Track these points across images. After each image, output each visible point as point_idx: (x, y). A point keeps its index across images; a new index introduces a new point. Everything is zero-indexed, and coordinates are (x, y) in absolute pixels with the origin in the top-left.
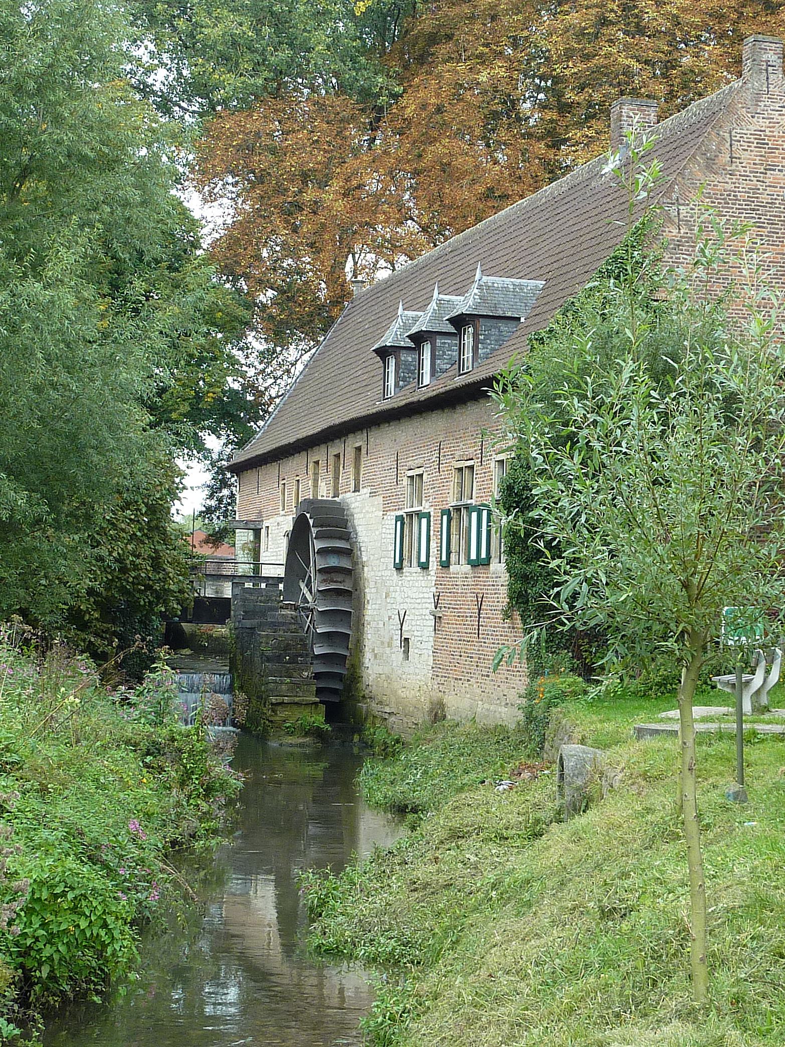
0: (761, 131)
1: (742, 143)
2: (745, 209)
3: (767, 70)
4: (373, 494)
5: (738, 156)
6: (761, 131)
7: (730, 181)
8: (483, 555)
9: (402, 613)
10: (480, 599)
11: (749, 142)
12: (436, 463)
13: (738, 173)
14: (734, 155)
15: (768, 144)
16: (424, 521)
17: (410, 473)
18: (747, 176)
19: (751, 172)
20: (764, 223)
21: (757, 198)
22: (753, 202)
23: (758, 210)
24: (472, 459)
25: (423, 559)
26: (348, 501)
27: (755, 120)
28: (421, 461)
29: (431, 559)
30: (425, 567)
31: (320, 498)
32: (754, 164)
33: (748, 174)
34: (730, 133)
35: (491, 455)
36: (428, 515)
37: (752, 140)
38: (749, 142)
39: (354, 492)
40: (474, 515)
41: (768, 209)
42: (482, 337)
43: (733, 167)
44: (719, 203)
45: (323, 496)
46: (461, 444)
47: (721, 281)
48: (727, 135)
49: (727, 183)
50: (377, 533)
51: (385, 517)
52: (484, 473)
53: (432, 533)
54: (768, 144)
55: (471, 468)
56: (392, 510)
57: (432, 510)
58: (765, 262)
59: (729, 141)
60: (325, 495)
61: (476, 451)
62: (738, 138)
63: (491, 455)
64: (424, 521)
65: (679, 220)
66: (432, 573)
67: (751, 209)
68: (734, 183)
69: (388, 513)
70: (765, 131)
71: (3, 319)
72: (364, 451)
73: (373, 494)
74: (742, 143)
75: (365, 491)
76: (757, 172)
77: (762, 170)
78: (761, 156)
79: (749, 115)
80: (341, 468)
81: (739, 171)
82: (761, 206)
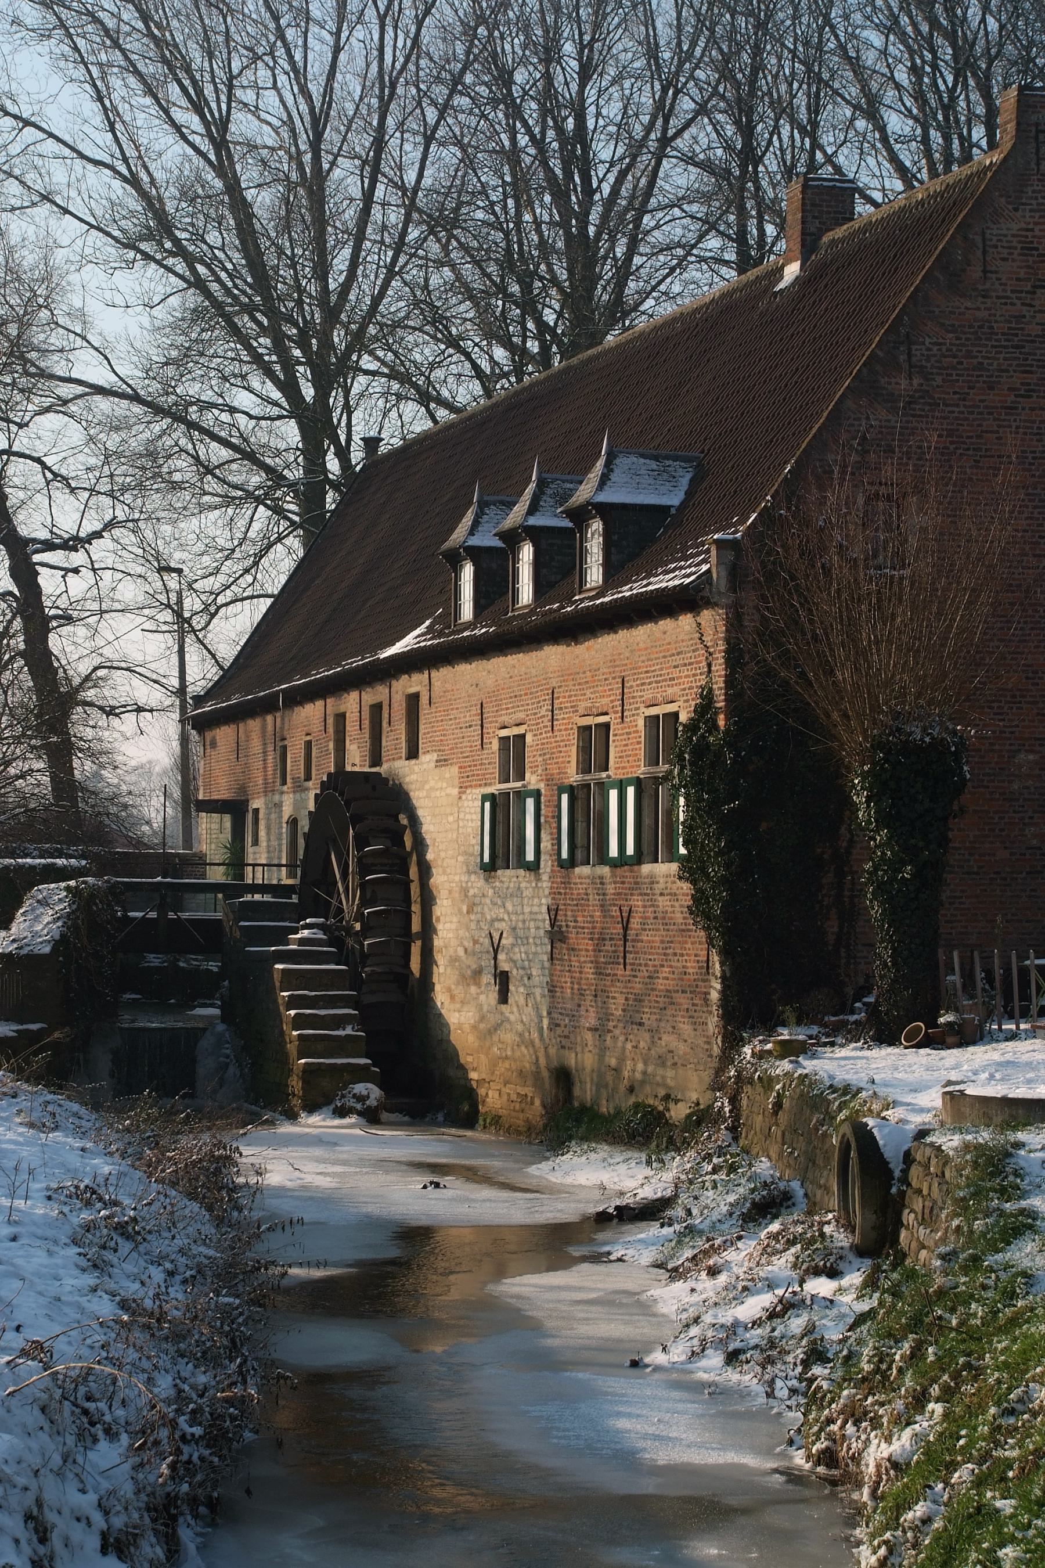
0: (1027, 230)
1: (1000, 249)
2: (1005, 347)
3: (1037, 138)
4: (441, 762)
5: (994, 268)
6: (1027, 230)
7: (982, 306)
8: (630, 850)
9: (496, 936)
10: (625, 915)
11: (1010, 248)
12: (546, 719)
13: (994, 294)
14: (989, 268)
15: (1037, 249)
16: (530, 803)
17: (504, 733)
18: (1008, 298)
19: (1012, 291)
20: (1032, 366)
21: (1022, 329)
22: (1017, 335)
23: (1023, 347)
24: (606, 714)
25: (530, 856)
26: (401, 772)
27: (1019, 214)
28: (521, 716)
29: (543, 858)
30: (534, 867)
31: (348, 768)
32: (1018, 279)
33: (1009, 294)
34: (983, 233)
35: (637, 709)
36: (537, 795)
37: (1014, 244)
38: (1010, 248)
39: (407, 759)
40: (613, 794)
41: (1037, 345)
42: (615, 537)
43: (988, 286)
44: (967, 339)
45: (354, 765)
46: (588, 692)
47: (971, 452)
48: (978, 239)
49: (978, 309)
50: (451, 819)
51: (464, 797)
52: (628, 733)
53: (542, 820)
54: (1037, 249)
55: (606, 726)
56: (476, 786)
57: (542, 786)
58: (1034, 422)
59: (981, 246)
60: (357, 762)
61: (612, 701)
62: (994, 242)
63: (637, 709)
64: (530, 803)
65: (911, 366)
66: (545, 877)
67: (1013, 347)
68: (989, 309)
69: (469, 791)
70: (1032, 230)
71: (1028, 1566)
72: (424, 700)
73: (441, 762)
74: (1000, 249)
75: (427, 759)
76: (1021, 292)
77: (1029, 288)
78: (1029, 267)
79: (1010, 207)
80: (385, 724)
81: (995, 291)
82: (1027, 341)
